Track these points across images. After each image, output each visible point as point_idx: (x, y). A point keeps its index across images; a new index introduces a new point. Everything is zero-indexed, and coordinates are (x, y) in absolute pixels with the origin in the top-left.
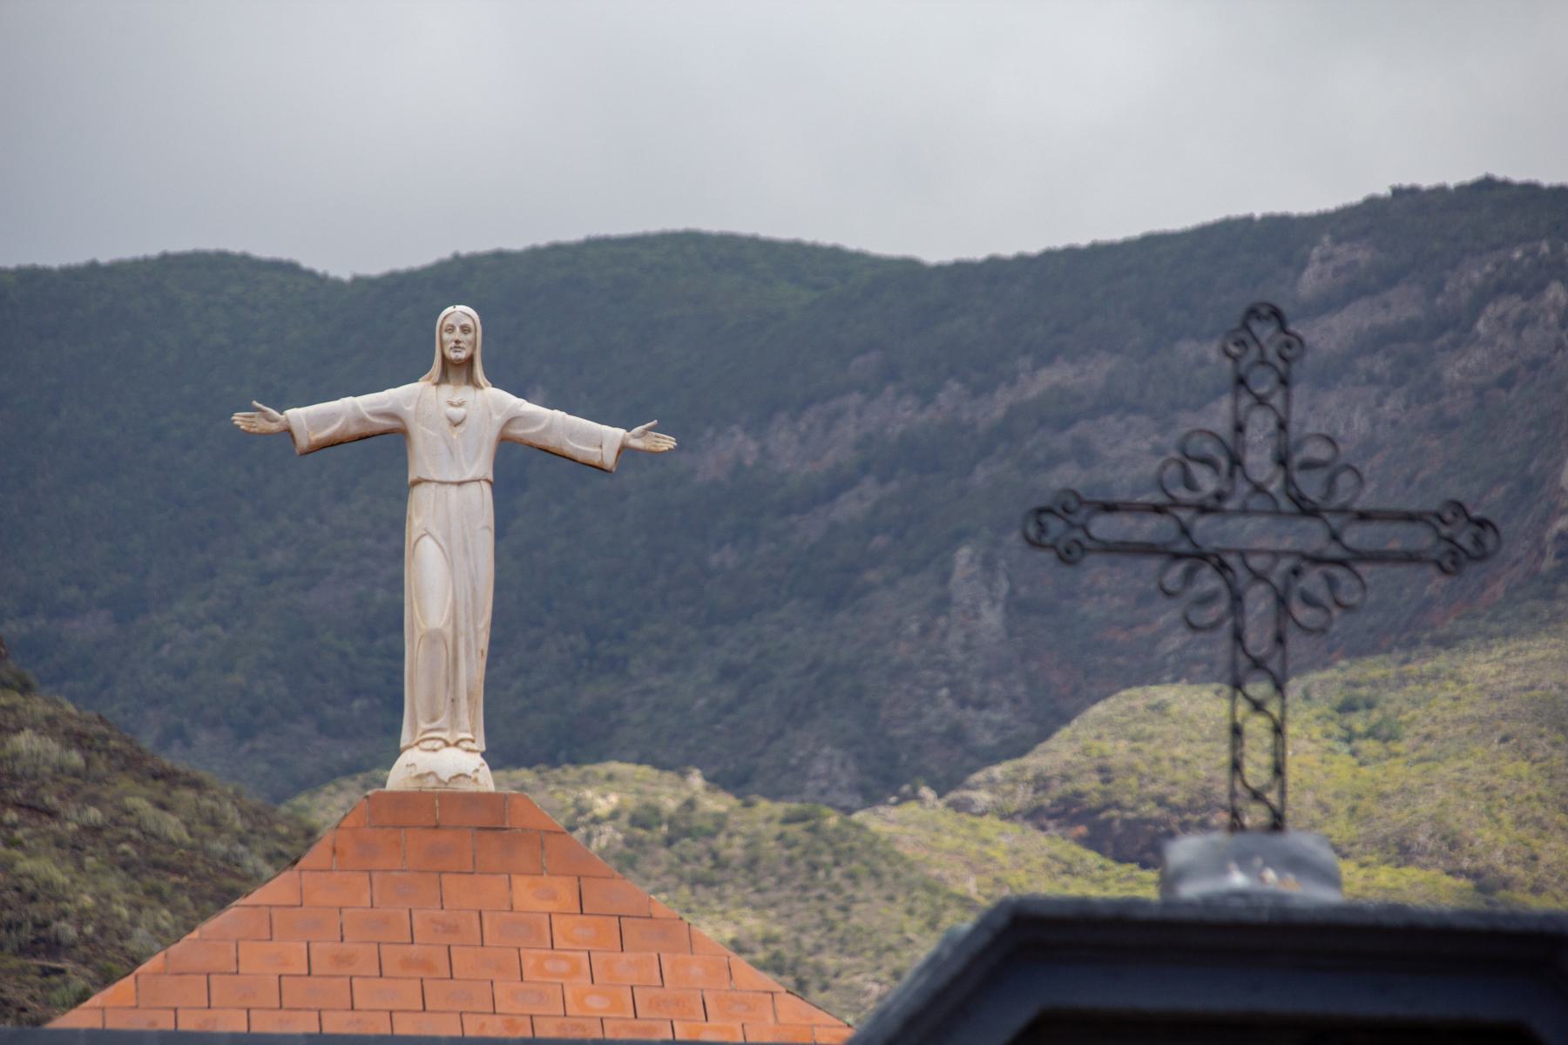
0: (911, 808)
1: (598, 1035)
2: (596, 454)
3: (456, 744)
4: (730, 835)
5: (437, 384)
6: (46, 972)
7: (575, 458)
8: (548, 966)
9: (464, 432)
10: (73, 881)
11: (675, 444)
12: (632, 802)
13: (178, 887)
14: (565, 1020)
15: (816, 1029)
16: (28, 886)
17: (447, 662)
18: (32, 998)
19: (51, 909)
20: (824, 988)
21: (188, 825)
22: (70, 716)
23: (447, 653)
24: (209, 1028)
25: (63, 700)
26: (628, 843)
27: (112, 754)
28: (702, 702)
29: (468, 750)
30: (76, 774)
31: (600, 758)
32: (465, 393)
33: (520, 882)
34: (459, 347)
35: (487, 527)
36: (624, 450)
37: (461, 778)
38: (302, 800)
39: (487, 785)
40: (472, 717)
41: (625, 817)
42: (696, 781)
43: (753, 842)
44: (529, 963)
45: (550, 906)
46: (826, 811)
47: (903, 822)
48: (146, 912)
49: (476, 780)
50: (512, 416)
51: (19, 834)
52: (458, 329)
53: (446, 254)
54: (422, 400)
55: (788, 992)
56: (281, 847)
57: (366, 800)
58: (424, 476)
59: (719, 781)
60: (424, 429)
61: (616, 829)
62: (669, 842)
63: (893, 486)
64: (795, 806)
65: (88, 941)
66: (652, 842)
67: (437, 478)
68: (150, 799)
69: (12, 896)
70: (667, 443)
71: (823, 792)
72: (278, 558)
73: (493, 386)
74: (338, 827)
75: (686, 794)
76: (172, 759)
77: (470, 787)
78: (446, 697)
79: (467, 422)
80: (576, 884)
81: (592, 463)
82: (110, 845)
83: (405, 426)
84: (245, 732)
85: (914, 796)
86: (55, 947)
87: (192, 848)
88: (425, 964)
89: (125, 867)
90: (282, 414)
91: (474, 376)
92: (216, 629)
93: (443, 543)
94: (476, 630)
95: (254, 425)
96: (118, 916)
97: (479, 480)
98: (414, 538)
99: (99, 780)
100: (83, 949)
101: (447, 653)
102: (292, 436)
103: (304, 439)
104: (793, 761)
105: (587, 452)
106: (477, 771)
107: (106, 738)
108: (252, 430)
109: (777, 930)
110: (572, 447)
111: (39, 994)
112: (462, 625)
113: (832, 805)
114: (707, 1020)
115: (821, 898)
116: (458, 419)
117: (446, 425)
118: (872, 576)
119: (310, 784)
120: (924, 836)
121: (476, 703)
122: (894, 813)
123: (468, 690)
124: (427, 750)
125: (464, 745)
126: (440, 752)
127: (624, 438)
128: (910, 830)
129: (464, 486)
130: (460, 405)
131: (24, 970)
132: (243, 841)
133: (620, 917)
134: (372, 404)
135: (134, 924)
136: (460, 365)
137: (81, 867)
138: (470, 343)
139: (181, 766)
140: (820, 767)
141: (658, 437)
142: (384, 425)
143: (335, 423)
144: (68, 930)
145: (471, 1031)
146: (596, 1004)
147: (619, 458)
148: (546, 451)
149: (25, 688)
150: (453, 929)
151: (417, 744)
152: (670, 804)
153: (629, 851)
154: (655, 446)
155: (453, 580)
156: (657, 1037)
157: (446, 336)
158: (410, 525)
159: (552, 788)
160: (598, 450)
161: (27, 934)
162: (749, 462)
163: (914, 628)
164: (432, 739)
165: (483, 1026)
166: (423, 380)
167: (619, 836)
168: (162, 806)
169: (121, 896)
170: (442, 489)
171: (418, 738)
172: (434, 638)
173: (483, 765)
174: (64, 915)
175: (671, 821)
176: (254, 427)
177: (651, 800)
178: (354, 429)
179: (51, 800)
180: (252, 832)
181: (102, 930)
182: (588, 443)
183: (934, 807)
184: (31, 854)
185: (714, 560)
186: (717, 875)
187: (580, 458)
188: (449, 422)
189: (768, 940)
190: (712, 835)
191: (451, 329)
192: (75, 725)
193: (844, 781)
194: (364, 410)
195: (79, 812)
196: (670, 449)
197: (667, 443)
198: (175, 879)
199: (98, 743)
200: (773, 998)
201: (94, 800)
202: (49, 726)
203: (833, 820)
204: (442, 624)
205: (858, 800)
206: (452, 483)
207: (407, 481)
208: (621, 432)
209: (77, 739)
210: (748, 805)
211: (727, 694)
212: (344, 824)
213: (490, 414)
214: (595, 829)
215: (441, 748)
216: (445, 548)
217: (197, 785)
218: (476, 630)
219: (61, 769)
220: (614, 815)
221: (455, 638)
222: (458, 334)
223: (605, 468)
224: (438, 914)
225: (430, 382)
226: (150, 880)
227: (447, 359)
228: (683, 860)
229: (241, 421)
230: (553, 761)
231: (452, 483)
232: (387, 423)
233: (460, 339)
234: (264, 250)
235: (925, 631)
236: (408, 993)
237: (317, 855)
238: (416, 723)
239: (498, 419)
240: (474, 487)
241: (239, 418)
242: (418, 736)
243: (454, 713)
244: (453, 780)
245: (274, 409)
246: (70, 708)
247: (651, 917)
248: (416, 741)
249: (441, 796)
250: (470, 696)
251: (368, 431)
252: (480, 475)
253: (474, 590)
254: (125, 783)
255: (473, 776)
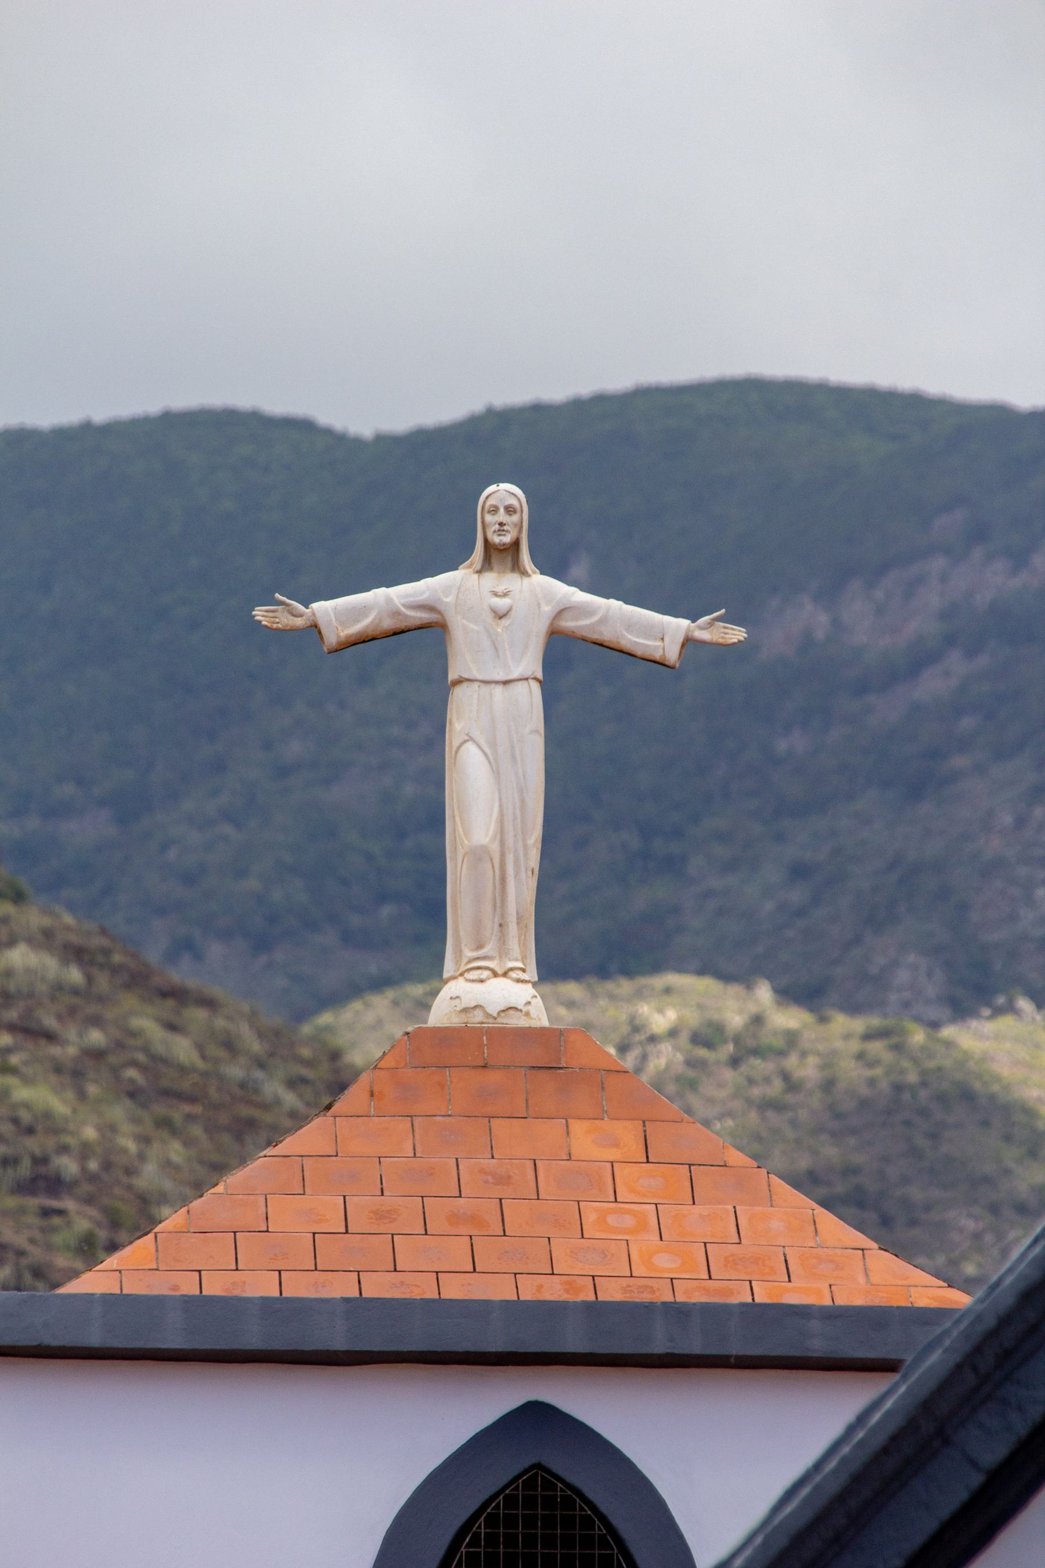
0: (1006, 1023)
1: (668, 1298)
2: (657, 647)
3: (505, 974)
4: (804, 1054)
5: (479, 572)
6: (46, 1213)
7: (633, 653)
8: (611, 1220)
9: (509, 625)
10: (75, 1111)
11: (746, 635)
12: (693, 1019)
13: (190, 1117)
14: (631, 1281)
15: (912, 1289)
16: (25, 1117)
17: (494, 883)
18: (32, 1241)
19: (51, 1143)
20: (913, 1223)
21: (200, 1048)
22: (68, 928)
23: (494, 872)
24: (237, 1292)
25: (58, 909)
26: (690, 1063)
27: (115, 970)
28: (769, 906)
29: (518, 981)
30: (75, 991)
31: (657, 968)
32: (511, 582)
33: (578, 1127)
34: (503, 530)
35: (537, 731)
36: (688, 642)
37: (511, 1012)
38: (326, 1018)
39: (540, 1020)
40: (523, 944)
41: (684, 1038)
42: (764, 993)
43: (828, 1062)
44: (590, 1218)
45: (613, 1154)
46: (911, 1026)
47: (998, 1037)
48: (156, 1146)
49: (527, 1014)
50: (563, 607)
51: (14, 1060)
52: (502, 510)
53: (478, 406)
54: (462, 590)
55: (880, 1248)
56: (305, 1072)
57: (406, 1038)
58: (465, 675)
59: (788, 995)
60: (464, 621)
61: (676, 1048)
62: (735, 1062)
63: (983, 661)
64: (875, 1021)
65: (92, 1178)
66: (718, 1062)
67: (480, 677)
68: (158, 1020)
69: (7, 1128)
70: (736, 634)
71: (906, 1005)
72: (294, 749)
73: (541, 574)
74: (375, 1068)
75: (753, 1008)
76: (181, 975)
77: (522, 1022)
78: (493, 922)
79: (513, 613)
80: (641, 1128)
81: (652, 658)
82: (115, 1071)
83: (445, 620)
84: (262, 944)
85: (1010, 1008)
86: (55, 1185)
87: (205, 1074)
88: (475, 1220)
89: (132, 1095)
90: (307, 608)
91: (521, 560)
92: (228, 829)
93: (488, 750)
94: (525, 847)
95: (277, 620)
96: (124, 1151)
97: (527, 679)
98: (456, 744)
99: (101, 999)
100: (86, 1188)
101: (494, 872)
102: (320, 632)
103: (334, 633)
104: (874, 970)
105: (647, 646)
106: (529, 1003)
107: (107, 952)
108: (275, 626)
109: (859, 1159)
110: (631, 641)
111: (38, 1236)
112: (510, 841)
113: (918, 1019)
114: (790, 1281)
115: (907, 1123)
116: (501, 612)
117: (489, 618)
118: (960, 762)
119: (335, 999)
120: (1023, 1054)
121: (526, 927)
122: (989, 1027)
123: (517, 914)
124: (473, 981)
125: (514, 975)
126: (488, 982)
127: (688, 630)
128: (1008, 1045)
129: (512, 685)
130: (505, 595)
131: (22, 1211)
132: (261, 1065)
133: (690, 1165)
134: (408, 596)
135: (142, 1157)
136: (504, 550)
137: (82, 1096)
138: (515, 525)
139: (192, 983)
140: (903, 976)
141: (725, 628)
142: (420, 618)
143: (367, 616)
144: (68, 1166)
145: (527, 1294)
146: (665, 1263)
147: (684, 651)
148: (601, 645)
149: (18, 897)
150: (504, 1180)
151: (462, 975)
152: (735, 1020)
153: (691, 1073)
154: (723, 638)
155: (500, 791)
156: (735, 1300)
157: (488, 518)
158: (450, 731)
159: (603, 1002)
160: (659, 643)
161: (25, 1169)
162: (820, 635)
163: (1008, 819)
164: (479, 968)
165: (540, 1287)
166: (464, 568)
167: (680, 1057)
168: (171, 1027)
169: (126, 1128)
170: (486, 689)
171: (463, 968)
172: (478, 855)
173: (535, 997)
174: (64, 1149)
175: (737, 1040)
176: (278, 623)
177: (716, 1017)
178: (388, 624)
179: (50, 1022)
180: (272, 1055)
181: (107, 1166)
182: (648, 637)
183: (1034, 1019)
184: (28, 1081)
185: (782, 746)
186: (790, 1098)
187: (639, 653)
188: (493, 615)
189: (850, 1171)
190: (782, 1053)
191: (494, 510)
192: (74, 939)
193: (931, 991)
194: (398, 602)
195: (80, 1035)
196: (740, 641)
197: (736, 634)
198: (187, 1108)
199: (100, 959)
200: (863, 1255)
201: (96, 1021)
202: (46, 939)
203: (918, 1036)
204: (487, 840)
205: (946, 1012)
206: (497, 682)
207: (447, 680)
208: (685, 623)
209: (76, 954)
210: (823, 1020)
211: (797, 896)
212: (382, 1065)
213: (539, 604)
214: (650, 1048)
215: (488, 978)
216: (491, 757)
217: (209, 1003)
218: (525, 847)
219: (59, 988)
220: (673, 1033)
221: (503, 855)
222: (502, 516)
223: (667, 663)
224: (487, 1163)
225: (471, 570)
226: (160, 1109)
227: (490, 544)
228: (751, 1081)
229: (263, 616)
230: (603, 973)
231: (497, 682)
232: (424, 616)
233: (504, 522)
234: (276, 406)
235: (1021, 822)
236: (457, 1253)
237: (353, 1099)
238: (461, 951)
239: (548, 609)
240: (522, 687)
241: (260, 613)
242: (463, 965)
243: (503, 939)
244: (502, 1014)
245: (293, 600)
246: (68, 919)
247: (725, 1166)
248: (460, 972)
249: (490, 1032)
250: (520, 919)
251: (403, 625)
252: (528, 673)
253: (523, 801)
254: (129, 1001)
255: (524, 1009)
